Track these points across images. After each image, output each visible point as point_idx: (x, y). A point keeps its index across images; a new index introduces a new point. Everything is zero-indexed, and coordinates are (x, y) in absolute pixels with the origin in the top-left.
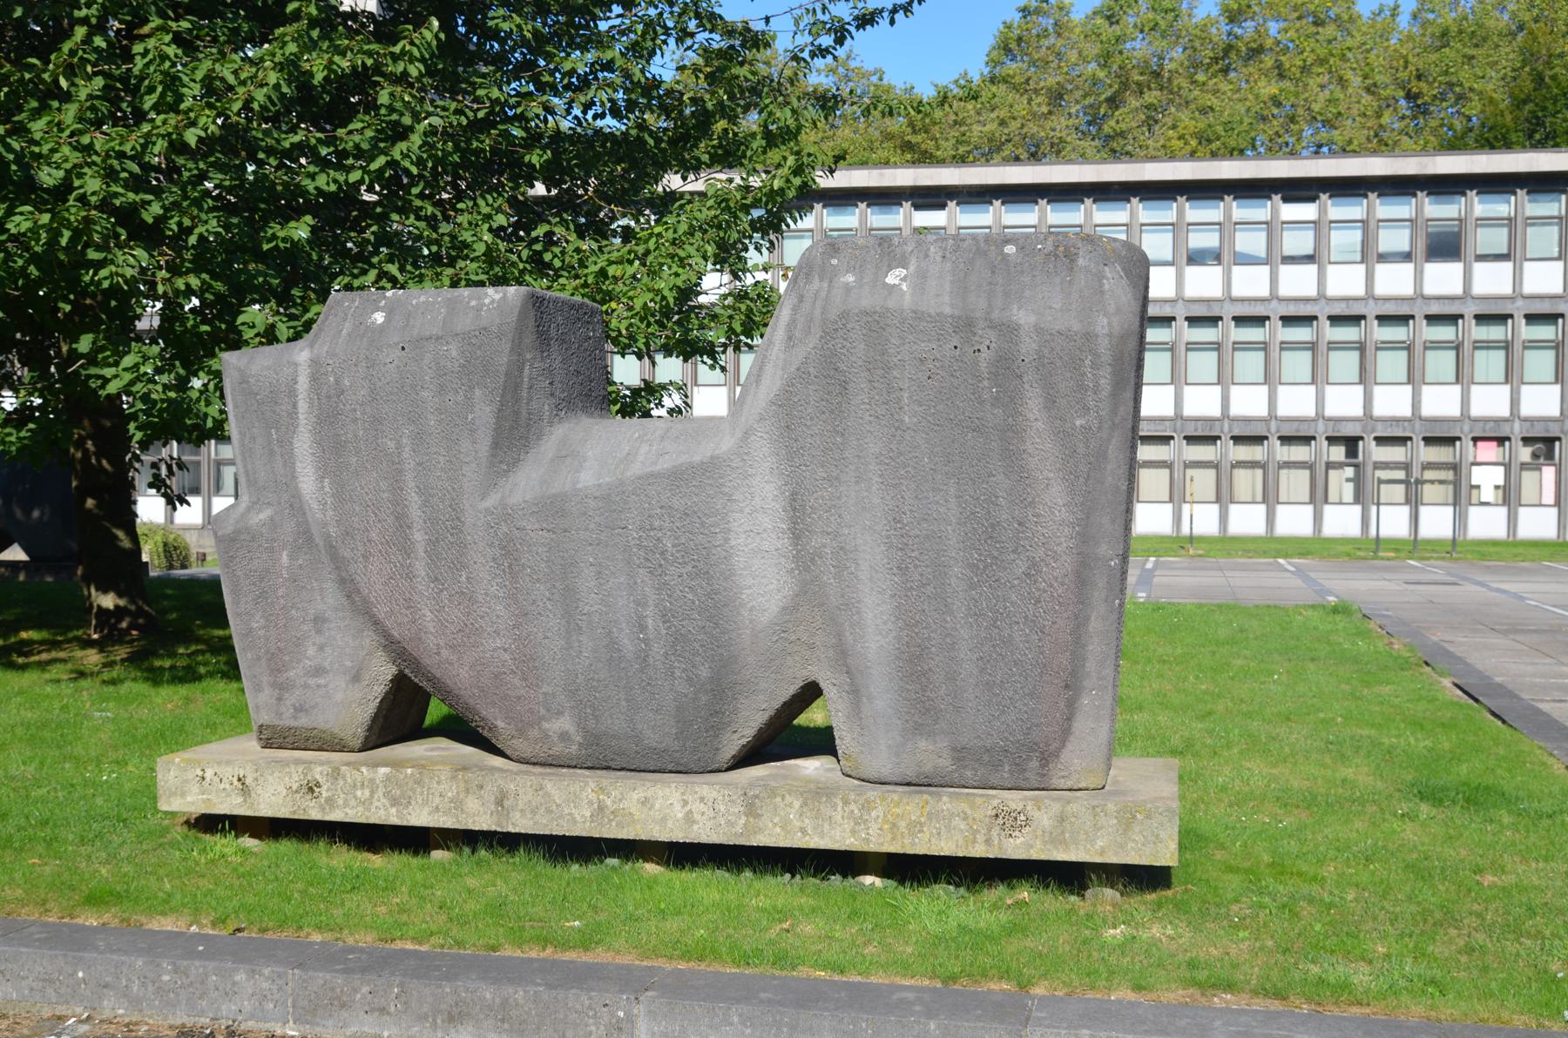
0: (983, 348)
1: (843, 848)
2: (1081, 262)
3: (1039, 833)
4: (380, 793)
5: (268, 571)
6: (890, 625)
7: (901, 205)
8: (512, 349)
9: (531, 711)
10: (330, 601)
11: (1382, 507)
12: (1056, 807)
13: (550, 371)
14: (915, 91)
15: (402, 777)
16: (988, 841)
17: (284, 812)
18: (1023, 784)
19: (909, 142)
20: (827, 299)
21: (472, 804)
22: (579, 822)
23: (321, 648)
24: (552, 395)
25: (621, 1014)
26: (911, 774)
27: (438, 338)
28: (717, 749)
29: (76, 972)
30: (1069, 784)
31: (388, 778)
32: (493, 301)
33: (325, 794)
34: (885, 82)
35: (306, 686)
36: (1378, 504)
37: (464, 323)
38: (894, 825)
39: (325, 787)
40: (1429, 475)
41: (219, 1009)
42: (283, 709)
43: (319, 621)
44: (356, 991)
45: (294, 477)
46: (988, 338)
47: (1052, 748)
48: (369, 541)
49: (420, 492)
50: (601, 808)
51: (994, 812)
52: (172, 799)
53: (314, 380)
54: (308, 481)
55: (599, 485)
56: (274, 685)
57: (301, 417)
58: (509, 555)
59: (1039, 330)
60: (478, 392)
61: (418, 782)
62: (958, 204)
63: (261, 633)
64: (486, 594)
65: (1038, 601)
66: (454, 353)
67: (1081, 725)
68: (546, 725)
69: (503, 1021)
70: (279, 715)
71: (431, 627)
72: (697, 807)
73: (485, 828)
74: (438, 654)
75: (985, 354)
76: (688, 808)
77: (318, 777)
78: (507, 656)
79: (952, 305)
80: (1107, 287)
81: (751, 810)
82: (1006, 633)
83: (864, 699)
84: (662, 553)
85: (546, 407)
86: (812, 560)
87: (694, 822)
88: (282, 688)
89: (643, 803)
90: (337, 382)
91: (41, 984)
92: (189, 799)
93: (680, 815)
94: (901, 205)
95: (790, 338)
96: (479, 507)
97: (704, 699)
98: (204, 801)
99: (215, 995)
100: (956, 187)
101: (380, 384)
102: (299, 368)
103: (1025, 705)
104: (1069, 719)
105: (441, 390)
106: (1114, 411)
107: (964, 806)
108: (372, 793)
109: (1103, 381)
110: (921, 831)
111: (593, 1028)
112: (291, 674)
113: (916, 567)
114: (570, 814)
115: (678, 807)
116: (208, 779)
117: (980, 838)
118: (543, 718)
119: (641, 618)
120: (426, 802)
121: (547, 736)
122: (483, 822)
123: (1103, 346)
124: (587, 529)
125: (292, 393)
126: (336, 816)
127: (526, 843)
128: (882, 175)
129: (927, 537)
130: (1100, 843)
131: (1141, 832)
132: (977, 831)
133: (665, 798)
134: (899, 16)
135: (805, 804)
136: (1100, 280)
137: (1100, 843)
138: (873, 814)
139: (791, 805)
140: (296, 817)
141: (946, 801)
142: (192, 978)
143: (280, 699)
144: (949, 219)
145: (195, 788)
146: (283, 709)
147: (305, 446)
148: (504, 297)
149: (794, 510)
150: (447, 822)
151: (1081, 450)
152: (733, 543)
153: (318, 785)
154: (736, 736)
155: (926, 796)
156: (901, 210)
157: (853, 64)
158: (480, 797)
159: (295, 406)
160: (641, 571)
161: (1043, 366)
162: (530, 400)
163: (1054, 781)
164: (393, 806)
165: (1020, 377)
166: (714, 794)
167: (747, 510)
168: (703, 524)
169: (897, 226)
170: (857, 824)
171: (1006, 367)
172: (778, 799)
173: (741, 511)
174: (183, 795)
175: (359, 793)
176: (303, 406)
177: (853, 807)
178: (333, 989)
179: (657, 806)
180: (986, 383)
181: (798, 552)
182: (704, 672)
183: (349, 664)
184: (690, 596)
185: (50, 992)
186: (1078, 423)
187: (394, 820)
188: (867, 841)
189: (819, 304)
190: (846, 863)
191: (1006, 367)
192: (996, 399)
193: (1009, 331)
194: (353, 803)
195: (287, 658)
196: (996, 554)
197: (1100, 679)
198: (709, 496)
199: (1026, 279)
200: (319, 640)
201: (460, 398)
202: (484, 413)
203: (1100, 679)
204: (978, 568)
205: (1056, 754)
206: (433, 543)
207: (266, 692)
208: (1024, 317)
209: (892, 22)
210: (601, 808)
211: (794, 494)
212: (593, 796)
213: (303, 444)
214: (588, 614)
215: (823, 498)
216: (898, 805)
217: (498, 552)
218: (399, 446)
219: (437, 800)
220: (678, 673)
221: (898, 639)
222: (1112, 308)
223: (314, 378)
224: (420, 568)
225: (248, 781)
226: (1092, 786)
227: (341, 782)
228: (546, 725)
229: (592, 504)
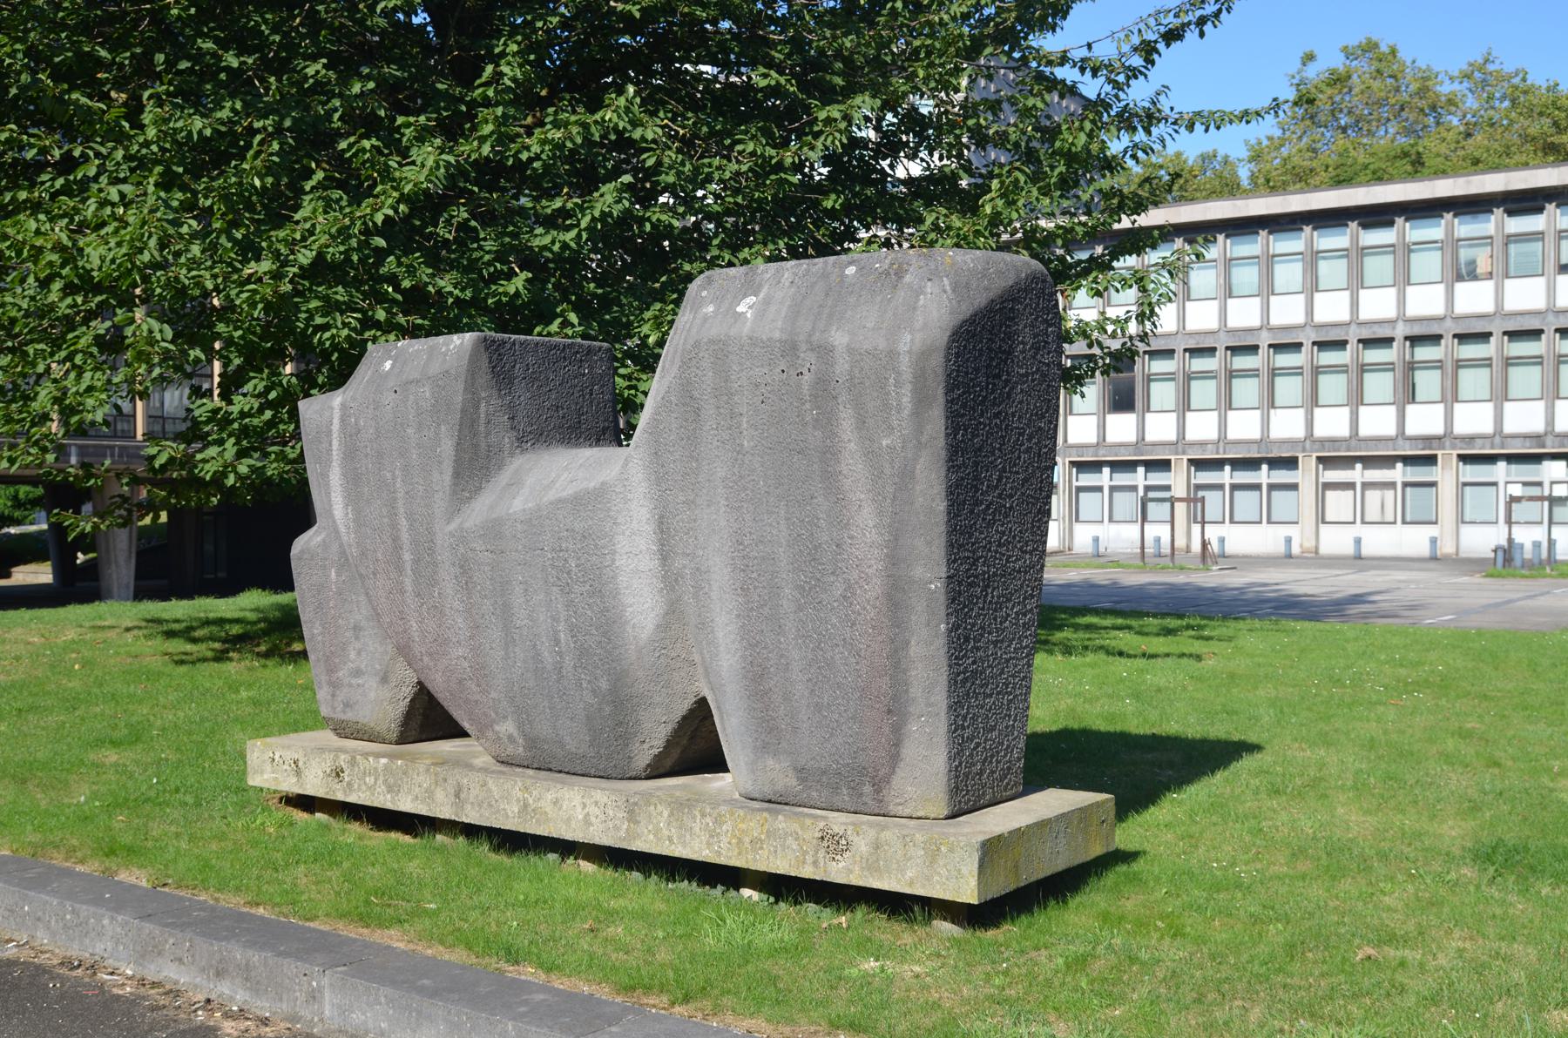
0: (805, 371)
1: (700, 859)
2: (908, 278)
3: (858, 859)
4: (380, 781)
7: (1492, 212)
8: (465, 389)
9: (485, 714)
11: (1207, 527)
12: (872, 833)
13: (511, 406)
14: (1559, 88)
16: (815, 863)
17: (320, 792)
18: (862, 808)
19: (1553, 143)
21: (440, 795)
24: (513, 428)
25: (314, 984)
26: (768, 791)
28: (630, 757)
30: (907, 812)
31: (386, 767)
34: (1529, 82)
35: (350, 685)
36: (1203, 523)
37: (435, 368)
38: (740, 841)
40: (1151, 495)
43: (357, 628)
46: (808, 359)
47: (881, 773)
50: (526, 806)
51: (820, 835)
58: (465, 568)
59: (850, 350)
60: (443, 428)
62: (1558, 206)
63: (320, 638)
65: (853, 624)
67: (910, 751)
68: (497, 728)
70: (334, 709)
72: (593, 810)
74: (421, 660)
75: (807, 377)
76: (586, 811)
79: (782, 330)
80: (921, 302)
81: (632, 816)
82: (828, 655)
84: (568, 573)
85: (507, 440)
86: (676, 580)
87: (591, 824)
89: (555, 803)
92: (265, 777)
93: (580, 817)
94: (1492, 212)
96: (445, 531)
97: (608, 709)
100: (1555, 188)
103: (850, 728)
104: (897, 744)
106: (919, 430)
107: (795, 826)
108: (376, 780)
109: (905, 400)
110: (761, 848)
111: (298, 994)
112: (340, 674)
113: (755, 588)
115: (579, 809)
117: (809, 859)
118: (493, 721)
119: (556, 632)
121: (499, 738)
122: (445, 812)
123: (905, 364)
128: (1468, 182)
129: (763, 558)
130: (909, 874)
131: (945, 866)
132: (806, 852)
133: (570, 800)
134: (1208, 28)
135: (671, 814)
136: (918, 296)
137: (909, 874)
138: (724, 827)
141: (782, 821)
143: (333, 696)
144: (1548, 222)
145: (269, 768)
146: (336, 704)
149: (662, 532)
150: (422, 810)
151: (888, 471)
154: (646, 746)
155: (766, 814)
156: (1493, 217)
157: (1491, 67)
158: (445, 789)
160: (555, 589)
161: (855, 386)
162: (488, 434)
163: (891, 807)
165: (835, 398)
166: (605, 799)
167: (627, 533)
168: (596, 545)
169: (1488, 234)
171: (824, 385)
172: (652, 808)
173: (624, 534)
174: (262, 773)
177: (708, 820)
179: (564, 807)
180: (808, 406)
181: (666, 572)
182: (604, 684)
183: (378, 667)
184: (589, 613)
186: (884, 443)
187: (389, 806)
190: (731, 877)
191: (824, 385)
192: (817, 420)
193: (825, 352)
194: (364, 788)
195: (337, 660)
196: (819, 576)
197: (929, 705)
199: (852, 300)
200: (358, 645)
202: (447, 447)
203: (929, 705)
204: (803, 588)
205: (887, 780)
206: (416, 561)
208: (839, 338)
209: (1202, 35)
210: (526, 806)
211: (661, 517)
212: (520, 794)
215: (683, 520)
216: (743, 821)
217: (458, 571)
219: (417, 790)
220: (585, 685)
221: (743, 657)
222: (918, 325)
223: (343, 420)
224: (409, 586)
225: (300, 764)
226: (933, 816)
228: (497, 728)
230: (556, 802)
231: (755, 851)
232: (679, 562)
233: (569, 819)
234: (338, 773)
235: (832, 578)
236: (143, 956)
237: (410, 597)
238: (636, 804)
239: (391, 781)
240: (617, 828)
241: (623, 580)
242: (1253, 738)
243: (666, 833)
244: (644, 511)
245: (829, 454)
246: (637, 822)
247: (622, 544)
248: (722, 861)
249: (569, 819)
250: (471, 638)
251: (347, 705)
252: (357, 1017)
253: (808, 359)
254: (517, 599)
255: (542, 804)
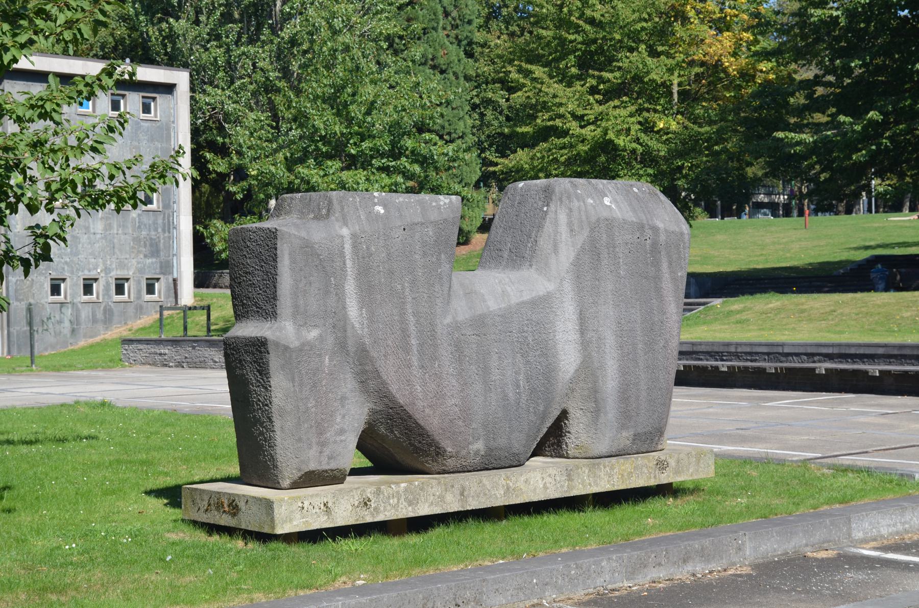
5: (317, 369)
6: (617, 376)
9: (465, 440)
10: (349, 386)
15: (413, 487)
17: (351, 521)
20: (586, 211)
21: (449, 497)
22: (499, 500)
23: (344, 417)
27: (423, 224)
29: (533, 580)
31: (406, 490)
32: (445, 204)
33: (373, 506)
35: (335, 442)
37: (434, 216)
38: (622, 475)
39: (373, 501)
41: (596, 582)
42: (322, 459)
43: (343, 399)
44: (649, 557)
45: (344, 308)
46: (649, 233)
48: (387, 346)
49: (414, 315)
50: (508, 488)
52: (284, 526)
53: (354, 247)
54: (353, 311)
55: (500, 309)
56: (318, 443)
57: (349, 270)
58: (458, 348)
60: (443, 256)
61: (422, 489)
64: (447, 374)
66: (431, 233)
69: (702, 557)
71: (420, 395)
72: (548, 480)
73: (456, 510)
74: (423, 411)
77: (369, 495)
78: (457, 409)
81: (570, 478)
83: (602, 414)
84: (528, 345)
87: (548, 488)
88: (323, 444)
90: (368, 248)
91: (516, 591)
92: (295, 523)
93: (541, 486)
95: (572, 230)
98: (304, 523)
99: (594, 575)
101: (392, 250)
102: (345, 239)
105: (425, 254)
108: (398, 500)
114: (495, 494)
115: (540, 481)
116: (305, 508)
117: (652, 476)
119: (518, 381)
120: (426, 500)
122: (454, 507)
124: (494, 333)
125: (342, 255)
126: (380, 518)
127: (453, 519)
132: (651, 473)
135: (590, 470)
139: (584, 472)
140: (358, 523)
142: (584, 569)
145: (298, 516)
147: (352, 289)
148: (451, 202)
149: (581, 319)
150: (437, 510)
152: (557, 337)
153: (369, 500)
159: (344, 264)
164: (409, 506)
166: (555, 472)
170: (610, 477)
171: (655, 245)
174: (291, 521)
175: (391, 501)
176: (349, 263)
178: (641, 559)
179: (532, 483)
185: (521, 594)
188: (613, 485)
189: (582, 213)
191: (655, 245)
193: (655, 229)
194: (389, 508)
195: (326, 425)
198: (547, 313)
201: (434, 260)
206: (421, 345)
207: (314, 449)
210: (508, 488)
212: (504, 482)
213: (350, 287)
214: (495, 381)
218: (403, 288)
219: (432, 498)
223: (355, 246)
224: (415, 361)
225: (329, 505)
227: (381, 496)
229: (498, 319)
230: (526, 481)
231: (629, 479)
232: (590, 334)
233: (535, 489)
234: (366, 503)
235: (659, 338)
236: (633, 573)
237: (416, 371)
238: (571, 470)
239: (411, 497)
240: (562, 486)
241: (559, 347)
242: (556, 413)
243: (588, 481)
244: (571, 308)
245: (657, 278)
246: (572, 480)
247: (560, 326)
248: (616, 488)
249: (535, 489)
250: (461, 391)
251: (330, 458)
252: (763, 548)
253: (649, 233)
254: (494, 362)
255: (518, 484)
